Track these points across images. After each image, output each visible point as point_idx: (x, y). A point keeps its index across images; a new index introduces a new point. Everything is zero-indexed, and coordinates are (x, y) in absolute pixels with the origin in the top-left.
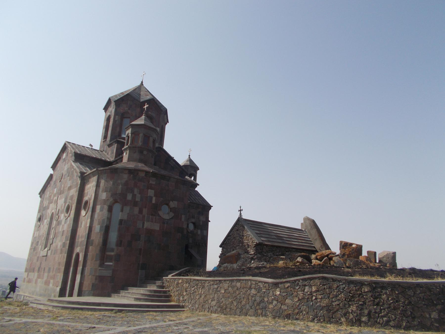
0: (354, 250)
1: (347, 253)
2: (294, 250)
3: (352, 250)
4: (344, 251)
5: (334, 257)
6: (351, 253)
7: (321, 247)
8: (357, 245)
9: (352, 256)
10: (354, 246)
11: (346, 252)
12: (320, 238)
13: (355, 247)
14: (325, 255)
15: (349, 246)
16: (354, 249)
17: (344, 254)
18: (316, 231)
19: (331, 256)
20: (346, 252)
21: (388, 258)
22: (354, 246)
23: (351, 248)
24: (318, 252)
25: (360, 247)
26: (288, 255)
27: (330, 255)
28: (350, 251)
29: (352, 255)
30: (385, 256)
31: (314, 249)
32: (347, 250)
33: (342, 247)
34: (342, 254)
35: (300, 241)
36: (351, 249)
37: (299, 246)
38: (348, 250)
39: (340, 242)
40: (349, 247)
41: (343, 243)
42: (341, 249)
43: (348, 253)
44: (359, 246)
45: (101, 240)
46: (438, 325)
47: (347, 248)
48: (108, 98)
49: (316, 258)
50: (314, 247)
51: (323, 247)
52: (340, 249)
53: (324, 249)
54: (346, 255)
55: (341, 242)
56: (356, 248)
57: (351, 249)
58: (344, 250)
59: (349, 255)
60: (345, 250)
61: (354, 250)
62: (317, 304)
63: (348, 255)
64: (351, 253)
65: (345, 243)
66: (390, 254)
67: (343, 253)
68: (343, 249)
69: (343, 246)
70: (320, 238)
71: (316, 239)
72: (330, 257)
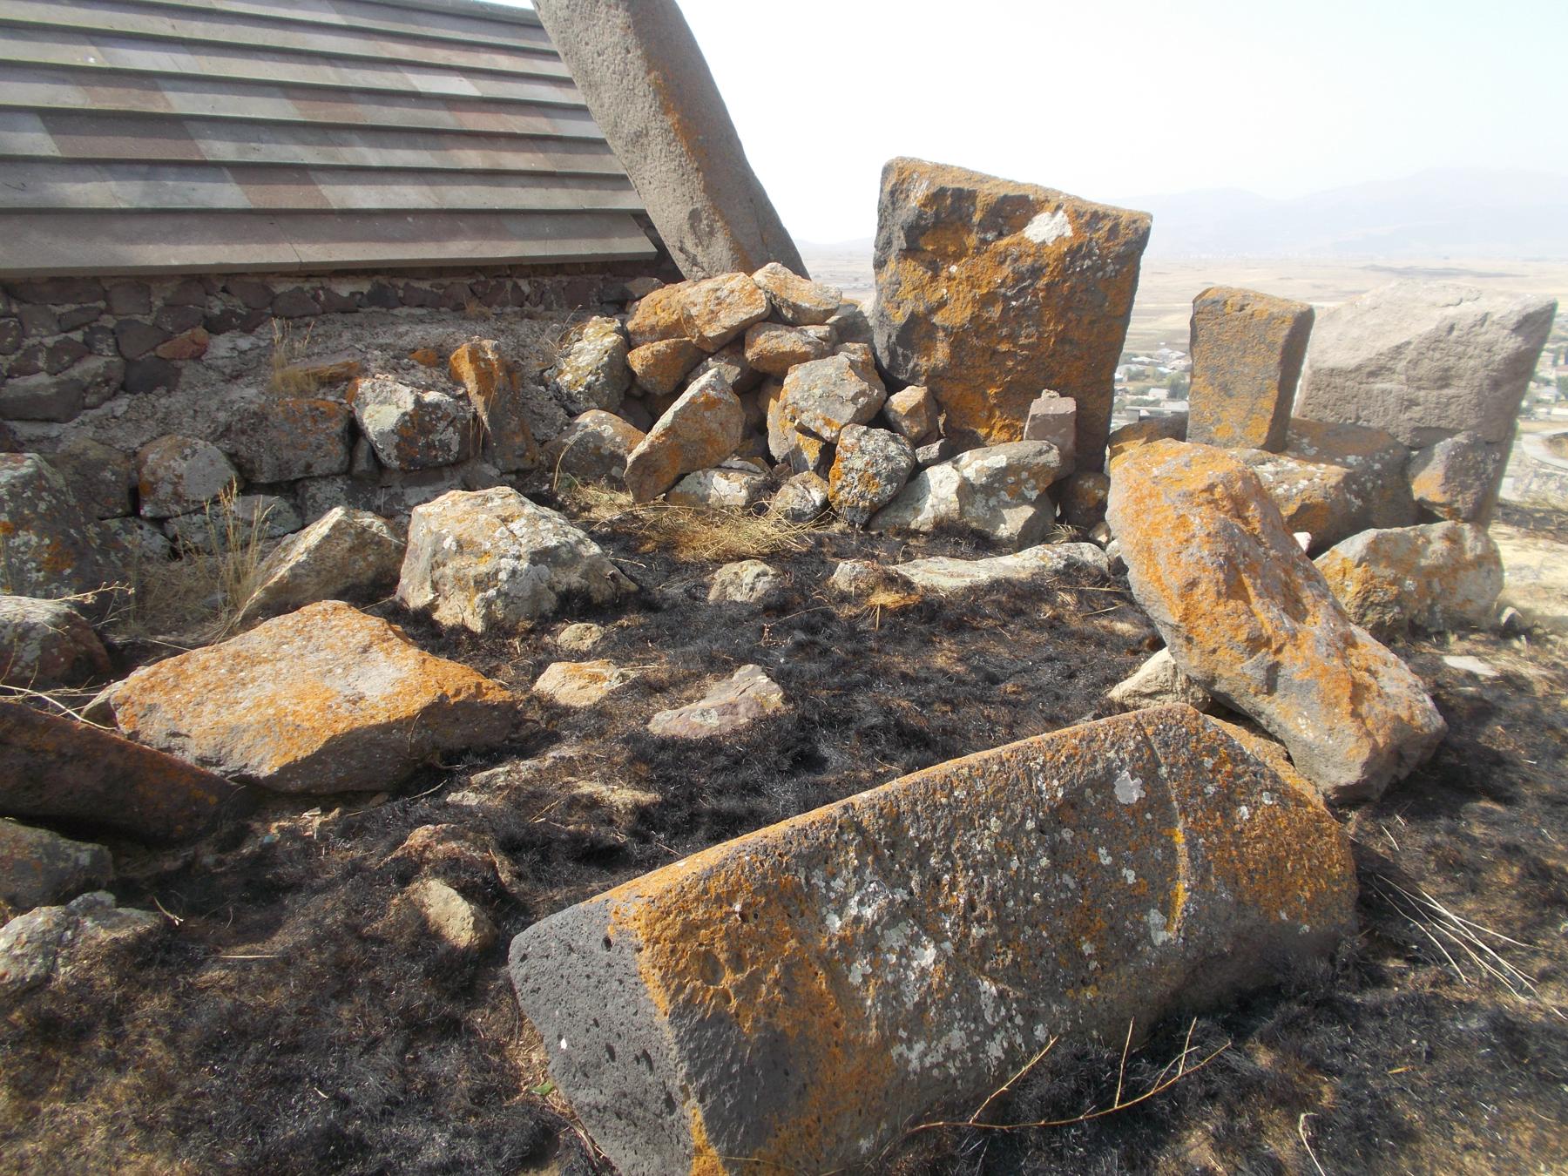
0: (1042, 283)
1: (957, 315)
2: (344, 289)
3: (1019, 277)
4: (919, 287)
5: (803, 358)
6: (995, 312)
7: (693, 228)
8: (1089, 218)
9: (1003, 347)
10: (1044, 230)
11: (942, 304)
12: (669, 121)
13: (1060, 239)
14: (712, 332)
15: (983, 227)
16: (1036, 272)
17: (914, 319)
18: (631, 40)
19: (773, 344)
20: (942, 304)
21: (1444, 379)
22: (1044, 230)
23: (1001, 259)
24: (673, 276)
25: (1117, 248)
26: (235, 377)
27: (768, 342)
28: (988, 300)
29: (1012, 338)
30: (1398, 350)
31: (638, 245)
32: (950, 278)
33: (900, 242)
34: (900, 318)
35: (472, 158)
36: (1007, 270)
37: (436, 237)
38: (972, 281)
39: (887, 170)
40: (984, 242)
41: (918, 194)
42: (891, 266)
43: (968, 313)
44: (1114, 231)
45: (19, 153)
46: (1446, 666)
47: (957, 257)
48: (1146, 210)
49: (610, 365)
50: (641, 220)
51: (711, 233)
52: (880, 264)
53: (720, 248)
54: (941, 334)
55: (893, 179)
56: (1060, 258)
57: (1007, 270)
58: (914, 272)
59: (978, 335)
60: (935, 277)
61: (1042, 283)
62: (388, 1151)
63: (958, 339)
64: (995, 312)
65: (937, 196)
66: (1489, 334)
67: (908, 308)
68: (910, 264)
69: (914, 232)
70: (669, 121)
71: (639, 137)
72: (761, 357)
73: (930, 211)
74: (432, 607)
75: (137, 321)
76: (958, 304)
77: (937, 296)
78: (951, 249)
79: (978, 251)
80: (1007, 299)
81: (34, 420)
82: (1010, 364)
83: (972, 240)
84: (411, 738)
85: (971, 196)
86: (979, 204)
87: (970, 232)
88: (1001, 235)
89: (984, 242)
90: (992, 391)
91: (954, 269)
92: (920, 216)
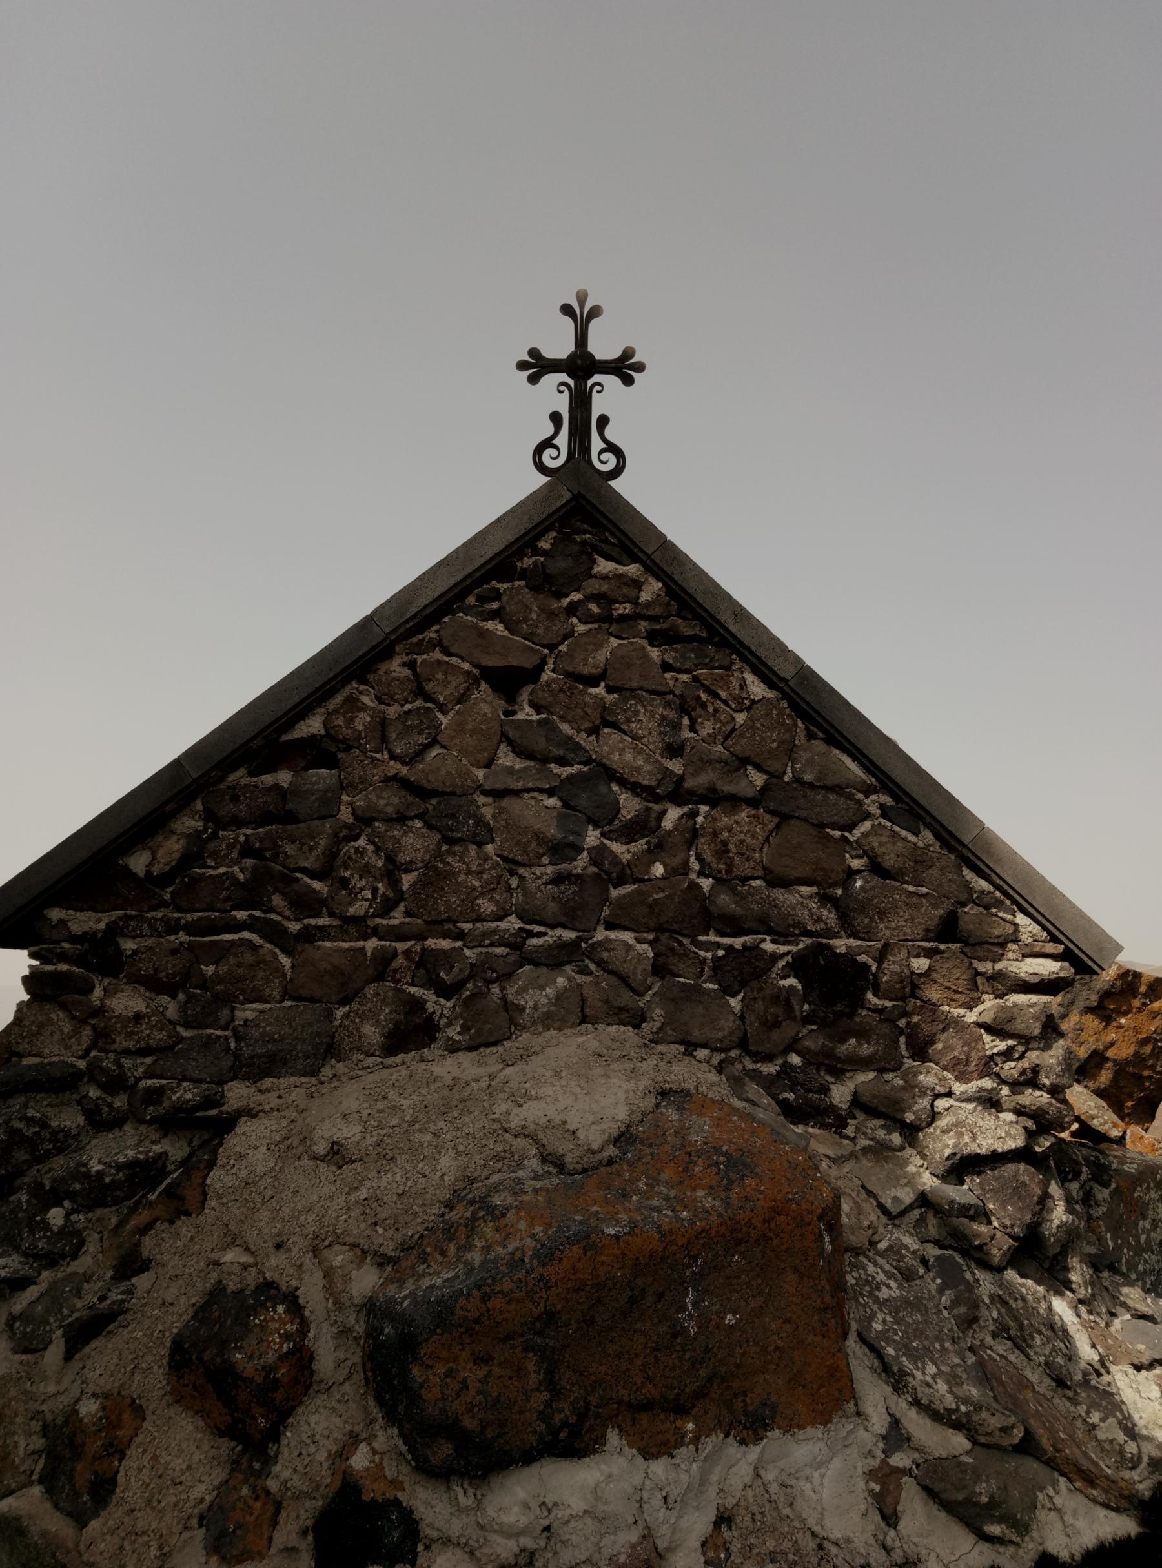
1: (1123, 1051)
6: (1148, 1049)
9: (1146, 1073)
11: (1112, 1044)
15: (1145, 995)
20: (1112, 1044)
32: (1120, 1027)
43: (1131, 1050)
47: (1125, 1014)
63: (1121, 1068)
64: (1148, 1049)
73: (1119, 983)
74: (265, 1278)
75: (891, 1000)
76: (1124, 1044)
77: (1109, 1039)
78: (1124, 1008)
79: (1140, 1010)
80: (1156, 1041)
81: (569, 928)
82: (1147, 1084)
83: (1136, 1003)
84: (160, 838)
85: (1137, 975)
86: (1144, 981)
87: (1135, 997)
88: (1152, 1002)
89: (1145, 1004)
90: (1130, 1104)
91: (1123, 1021)
92: (1113, 986)
